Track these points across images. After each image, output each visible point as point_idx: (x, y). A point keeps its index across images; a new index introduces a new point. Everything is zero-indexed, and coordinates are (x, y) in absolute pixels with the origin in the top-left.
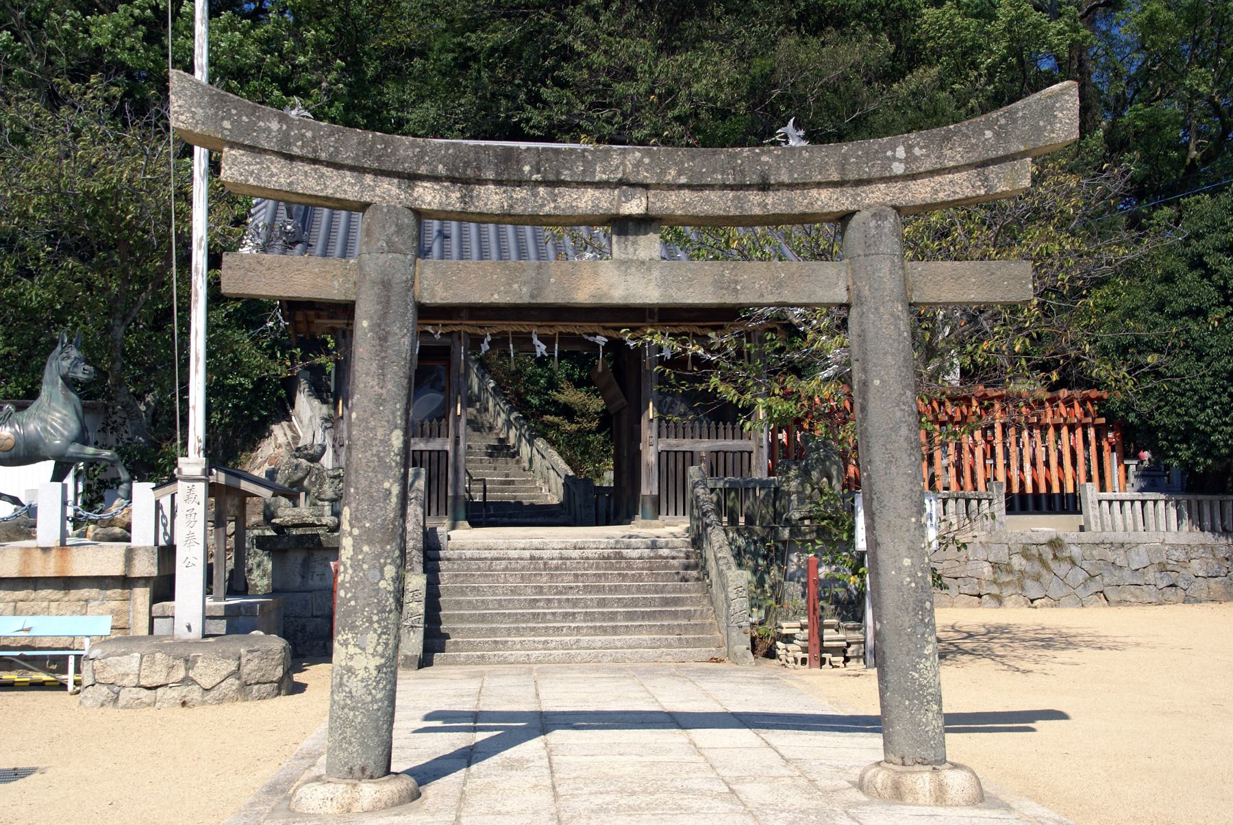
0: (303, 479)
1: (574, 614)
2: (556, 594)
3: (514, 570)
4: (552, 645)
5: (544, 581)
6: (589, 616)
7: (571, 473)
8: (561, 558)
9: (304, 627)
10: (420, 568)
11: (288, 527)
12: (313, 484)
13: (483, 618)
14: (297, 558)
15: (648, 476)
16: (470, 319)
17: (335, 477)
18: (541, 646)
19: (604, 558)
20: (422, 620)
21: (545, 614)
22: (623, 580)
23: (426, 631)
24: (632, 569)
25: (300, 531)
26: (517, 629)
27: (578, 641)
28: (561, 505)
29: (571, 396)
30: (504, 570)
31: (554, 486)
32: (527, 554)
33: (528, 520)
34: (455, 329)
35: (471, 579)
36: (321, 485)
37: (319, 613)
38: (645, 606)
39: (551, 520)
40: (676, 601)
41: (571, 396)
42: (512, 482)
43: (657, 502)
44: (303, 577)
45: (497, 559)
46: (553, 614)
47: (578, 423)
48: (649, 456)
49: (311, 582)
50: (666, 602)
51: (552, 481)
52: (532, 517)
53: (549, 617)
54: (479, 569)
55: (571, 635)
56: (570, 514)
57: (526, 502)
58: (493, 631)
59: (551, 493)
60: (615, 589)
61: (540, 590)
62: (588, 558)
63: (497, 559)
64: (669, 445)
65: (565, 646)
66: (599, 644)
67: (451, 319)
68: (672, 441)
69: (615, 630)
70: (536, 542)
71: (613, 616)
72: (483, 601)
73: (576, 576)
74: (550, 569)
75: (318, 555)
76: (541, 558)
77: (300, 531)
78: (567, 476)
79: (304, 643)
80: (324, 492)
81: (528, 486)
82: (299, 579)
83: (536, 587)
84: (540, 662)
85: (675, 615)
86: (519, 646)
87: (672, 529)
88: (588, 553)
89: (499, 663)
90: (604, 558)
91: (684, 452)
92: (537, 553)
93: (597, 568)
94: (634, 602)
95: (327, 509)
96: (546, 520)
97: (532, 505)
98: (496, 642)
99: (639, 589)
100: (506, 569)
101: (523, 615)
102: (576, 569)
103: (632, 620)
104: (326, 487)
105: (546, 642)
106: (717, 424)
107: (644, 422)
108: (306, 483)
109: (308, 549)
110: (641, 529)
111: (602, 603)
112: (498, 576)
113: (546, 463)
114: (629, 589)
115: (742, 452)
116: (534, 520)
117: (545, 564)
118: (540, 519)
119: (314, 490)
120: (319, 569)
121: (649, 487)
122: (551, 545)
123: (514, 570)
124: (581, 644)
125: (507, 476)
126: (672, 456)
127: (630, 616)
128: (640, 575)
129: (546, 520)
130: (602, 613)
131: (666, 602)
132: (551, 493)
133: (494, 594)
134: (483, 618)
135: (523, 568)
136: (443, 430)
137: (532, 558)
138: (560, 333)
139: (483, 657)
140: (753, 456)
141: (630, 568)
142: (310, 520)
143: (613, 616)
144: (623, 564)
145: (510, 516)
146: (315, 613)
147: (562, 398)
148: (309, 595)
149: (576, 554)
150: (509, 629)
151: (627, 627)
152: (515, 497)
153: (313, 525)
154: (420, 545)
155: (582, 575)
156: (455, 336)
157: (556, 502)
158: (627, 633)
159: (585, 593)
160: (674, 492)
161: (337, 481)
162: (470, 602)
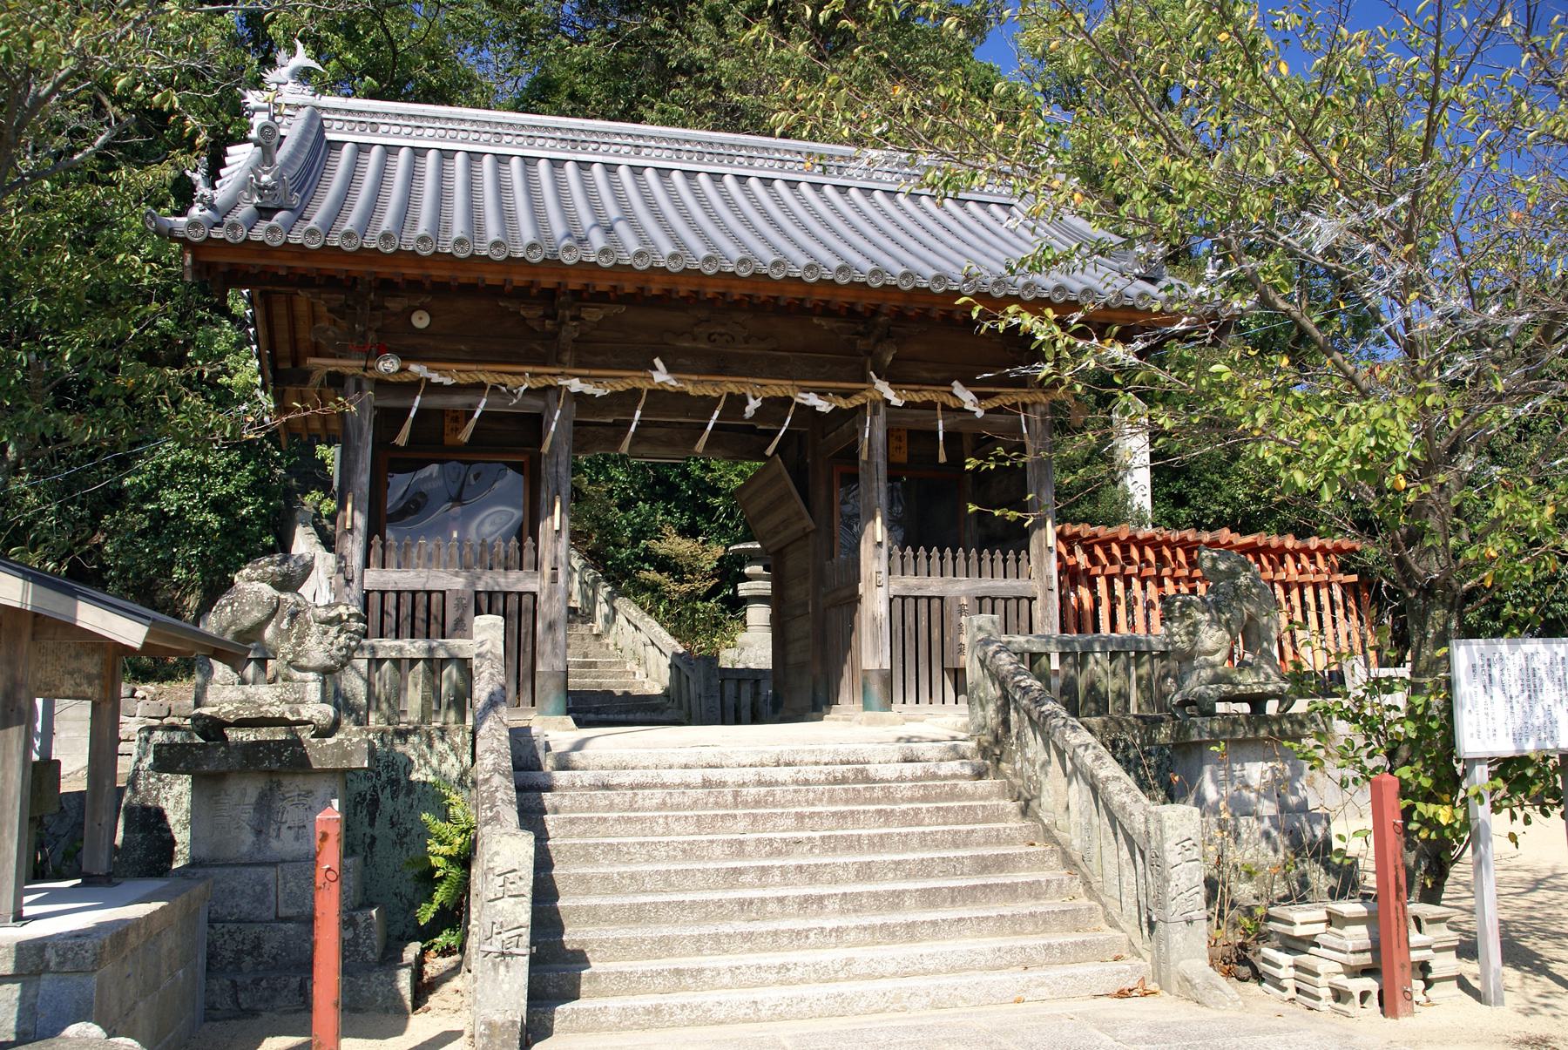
0: (260, 626)
1: (821, 898)
2: (770, 855)
3: (678, 807)
4: (796, 974)
5: (739, 830)
6: (851, 903)
7: (681, 650)
8: (760, 783)
9: (257, 945)
10: (511, 816)
11: (229, 725)
12: (283, 635)
13: (638, 914)
14: (244, 793)
15: (875, 637)
16: (577, 366)
17: (330, 622)
18: (772, 977)
19: (836, 781)
20: (526, 939)
21: (763, 901)
22: (887, 824)
23: (534, 961)
24: (894, 801)
25: (248, 735)
26: (716, 938)
27: (849, 962)
28: (667, 693)
29: (675, 545)
30: (658, 809)
31: (653, 670)
32: (695, 776)
33: (623, 717)
34: (551, 381)
35: (601, 828)
36: (301, 638)
37: (292, 912)
38: (945, 874)
39: (655, 717)
40: (1001, 863)
41: (675, 545)
42: (593, 665)
43: (887, 679)
44: (259, 833)
45: (642, 786)
46: (781, 900)
47: (688, 581)
48: (875, 602)
49: (274, 844)
50: (983, 865)
51: (651, 663)
52: (627, 712)
53: (771, 907)
54: (611, 807)
55: (825, 946)
56: (680, 707)
57: (618, 692)
58: (666, 945)
59: (653, 678)
60: (881, 843)
61: (739, 848)
62: (807, 782)
63: (642, 786)
64: (906, 587)
65: (825, 975)
66: (892, 968)
67: (544, 365)
68: (910, 580)
69: (911, 931)
70: (708, 755)
71: (895, 900)
72: (632, 877)
73: (800, 817)
74: (746, 804)
75: (294, 785)
76: (723, 784)
77: (248, 735)
78: (675, 654)
79: (256, 982)
80: (306, 653)
81: (615, 669)
82: (248, 838)
83: (730, 843)
84: (781, 1017)
85: (1011, 891)
86: (727, 979)
87: (943, 722)
88: (810, 772)
89: (693, 1023)
90: (836, 781)
91: (930, 598)
92: (714, 775)
93: (832, 801)
94: (925, 869)
95: (313, 688)
96: (648, 717)
97: (626, 693)
98: (678, 972)
99: (924, 841)
100: (663, 806)
101: (720, 904)
102: (792, 803)
103: (932, 905)
104: (311, 642)
105: (784, 967)
106: (980, 553)
107: (866, 549)
108: (269, 633)
109: (271, 772)
110: (845, 733)
111: (865, 872)
112: (653, 820)
113: (642, 637)
114: (905, 842)
115: (1018, 599)
116: (631, 717)
117: (736, 795)
118: (639, 716)
119: (285, 648)
120: (292, 815)
121: (872, 651)
122: (734, 760)
123: (678, 807)
124: (856, 969)
125: (586, 656)
126: (910, 603)
127: (929, 898)
128: (917, 812)
129: (648, 717)
130: (875, 895)
131: (983, 865)
132: (653, 678)
133: (651, 859)
134: (638, 914)
135: (694, 805)
136: (528, 556)
137: (707, 784)
138: (730, 395)
139: (657, 1010)
140: (1037, 605)
141: (889, 797)
142: (275, 711)
143: (895, 900)
144: (878, 793)
145: (598, 711)
146: (283, 911)
147: (661, 548)
148: (270, 874)
149: (784, 774)
150: (699, 939)
151: (934, 923)
152: (600, 685)
153: (280, 721)
154: (507, 764)
155: (812, 815)
156: (551, 395)
157: (658, 690)
158: (934, 936)
159: (825, 852)
160: (926, 657)
161: (334, 630)
162: (606, 878)
